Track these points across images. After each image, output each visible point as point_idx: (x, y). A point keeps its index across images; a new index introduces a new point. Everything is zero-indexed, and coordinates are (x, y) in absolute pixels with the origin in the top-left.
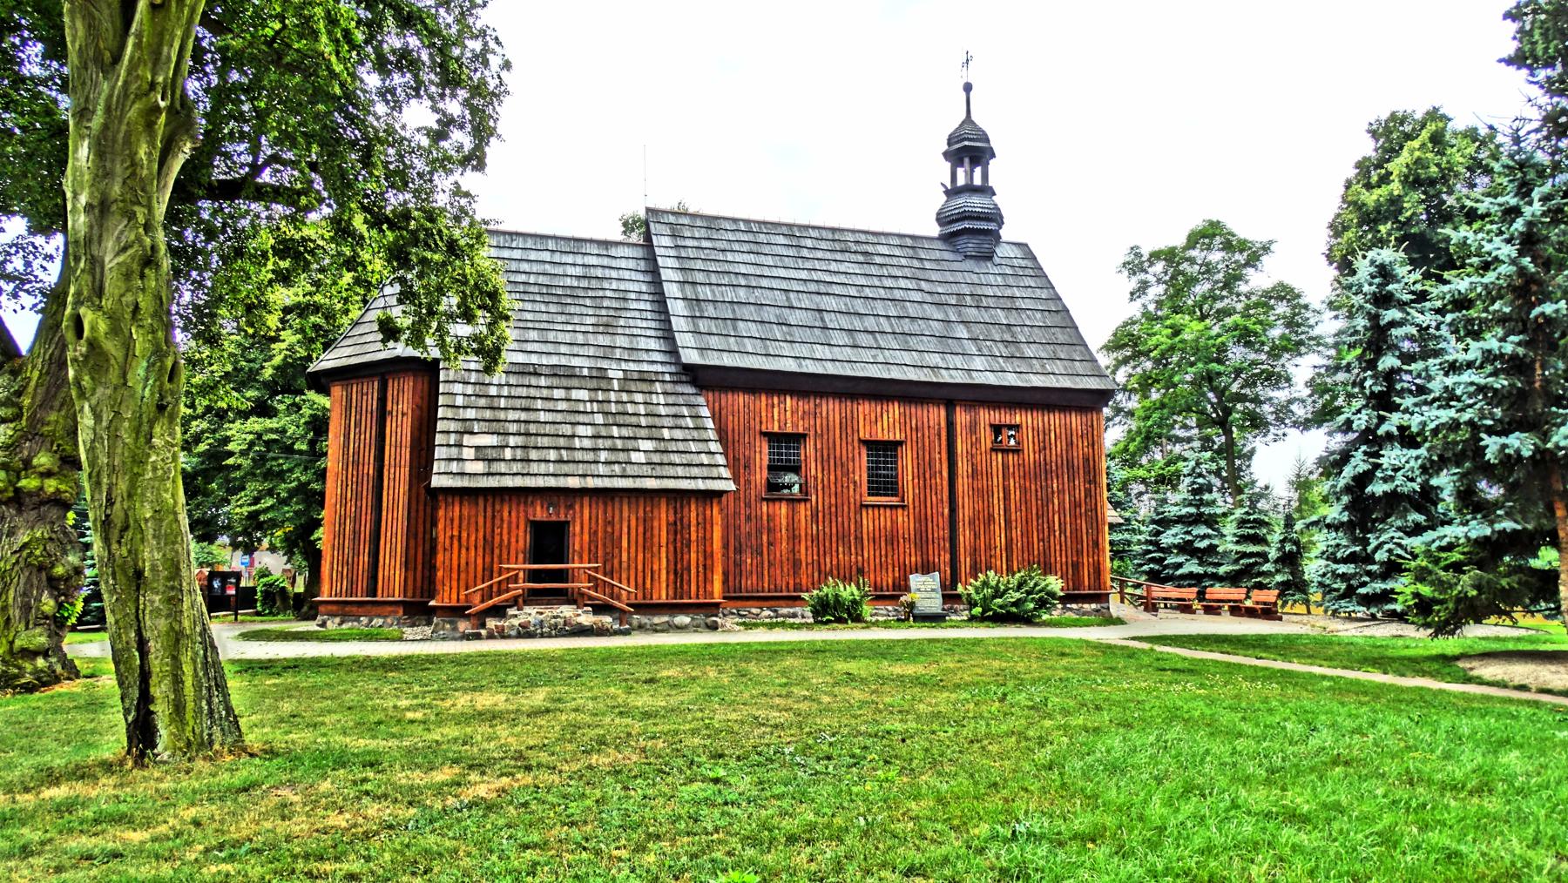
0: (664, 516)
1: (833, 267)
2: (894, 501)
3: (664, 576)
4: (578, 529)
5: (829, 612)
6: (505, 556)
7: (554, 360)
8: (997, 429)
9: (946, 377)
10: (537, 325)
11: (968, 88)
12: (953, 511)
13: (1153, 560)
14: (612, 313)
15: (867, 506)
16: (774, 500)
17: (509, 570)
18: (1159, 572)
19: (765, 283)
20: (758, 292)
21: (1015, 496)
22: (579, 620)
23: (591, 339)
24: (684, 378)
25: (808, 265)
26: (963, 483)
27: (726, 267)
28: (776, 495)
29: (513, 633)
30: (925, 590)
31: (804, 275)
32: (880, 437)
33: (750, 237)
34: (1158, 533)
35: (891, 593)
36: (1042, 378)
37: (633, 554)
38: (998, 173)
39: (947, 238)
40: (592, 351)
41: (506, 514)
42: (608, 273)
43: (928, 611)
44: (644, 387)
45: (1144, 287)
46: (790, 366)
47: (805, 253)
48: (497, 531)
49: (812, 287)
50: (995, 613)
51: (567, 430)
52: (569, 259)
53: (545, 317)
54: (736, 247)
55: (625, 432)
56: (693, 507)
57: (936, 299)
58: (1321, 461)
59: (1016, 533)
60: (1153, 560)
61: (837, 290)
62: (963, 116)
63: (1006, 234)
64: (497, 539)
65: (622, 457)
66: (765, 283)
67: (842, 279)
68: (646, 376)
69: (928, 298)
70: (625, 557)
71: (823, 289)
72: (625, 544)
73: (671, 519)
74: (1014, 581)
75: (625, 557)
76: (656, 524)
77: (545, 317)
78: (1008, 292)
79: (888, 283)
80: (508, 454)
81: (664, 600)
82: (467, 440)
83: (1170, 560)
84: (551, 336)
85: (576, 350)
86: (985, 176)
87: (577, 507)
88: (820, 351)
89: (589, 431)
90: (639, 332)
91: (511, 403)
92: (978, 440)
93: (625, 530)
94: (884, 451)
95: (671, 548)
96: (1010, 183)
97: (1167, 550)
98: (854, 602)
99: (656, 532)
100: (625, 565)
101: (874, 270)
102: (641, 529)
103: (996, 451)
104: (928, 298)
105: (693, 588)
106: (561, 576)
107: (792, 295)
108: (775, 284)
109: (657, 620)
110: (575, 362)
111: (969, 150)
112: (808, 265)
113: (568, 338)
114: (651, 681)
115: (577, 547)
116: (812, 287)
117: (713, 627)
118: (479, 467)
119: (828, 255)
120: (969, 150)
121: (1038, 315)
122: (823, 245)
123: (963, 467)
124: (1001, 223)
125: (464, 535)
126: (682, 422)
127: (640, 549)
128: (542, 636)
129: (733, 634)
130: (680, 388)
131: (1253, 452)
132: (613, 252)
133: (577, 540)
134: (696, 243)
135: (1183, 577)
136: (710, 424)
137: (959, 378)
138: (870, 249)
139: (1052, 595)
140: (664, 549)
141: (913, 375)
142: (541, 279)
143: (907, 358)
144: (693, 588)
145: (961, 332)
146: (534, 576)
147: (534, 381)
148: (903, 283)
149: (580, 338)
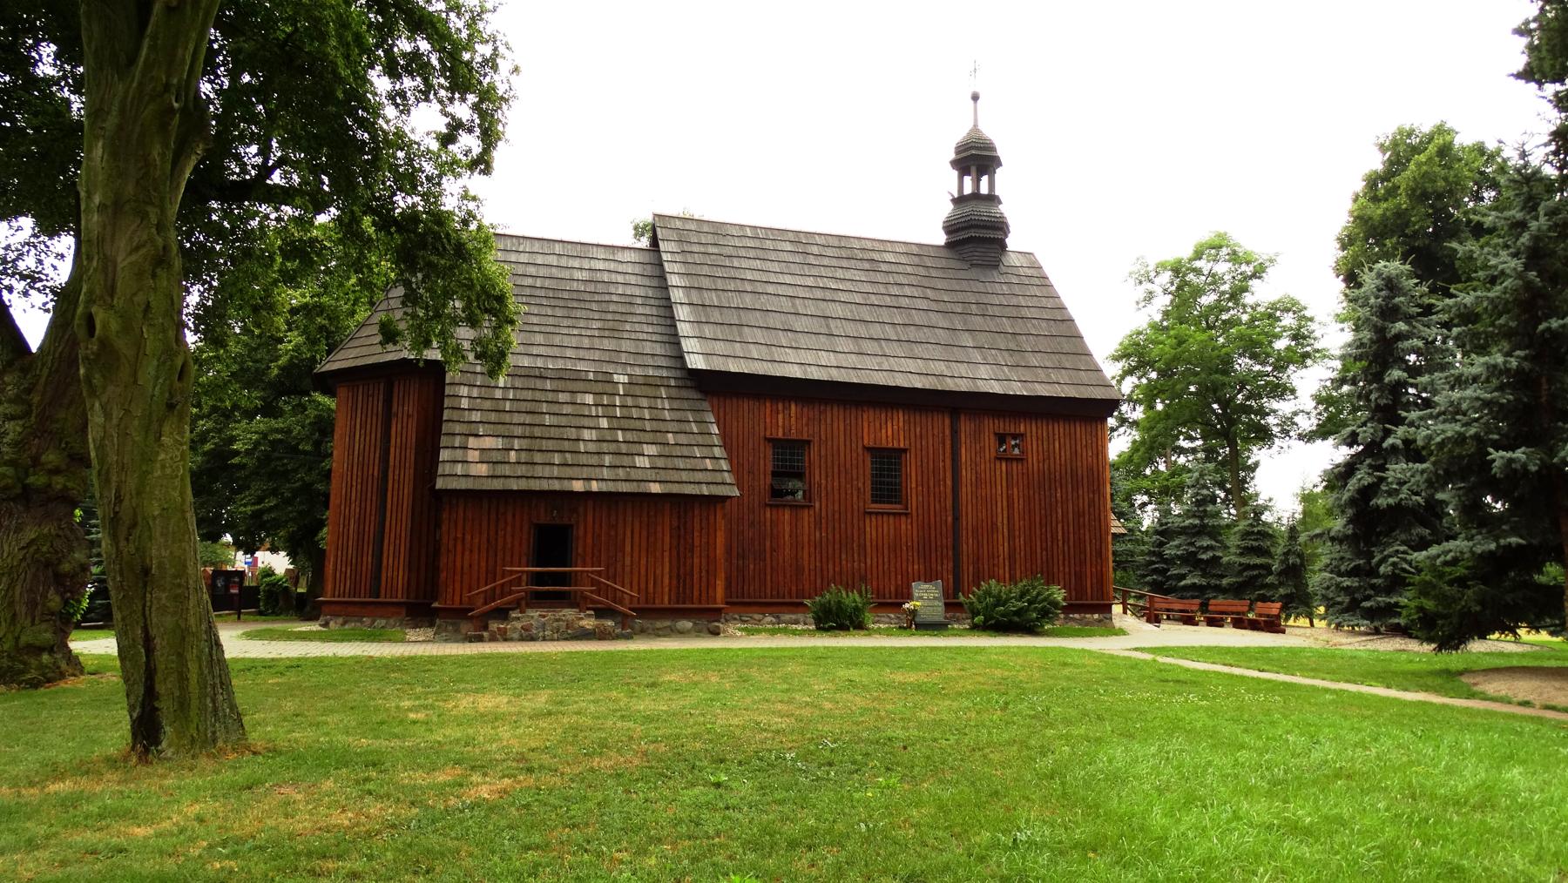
0: (667, 519)
1: (840, 274)
2: (897, 508)
3: (666, 581)
4: (581, 533)
5: (836, 620)
6: (508, 558)
7: (560, 364)
10: (543, 329)
11: (975, 98)
12: (956, 519)
13: (1155, 571)
14: (618, 317)
16: (777, 506)
17: (512, 572)
18: (1163, 583)
19: (770, 289)
20: (763, 298)
21: (1019, 505)
22: (583, 623)
23: (597, 343)
24: (689, 383)
25: (814, 271)
26: (965, 491)
27: (733, 273)
28: (778, 501)
29: (516, 636)
30: (926, 597)
31: (810, 282)
32: (884, 445)
33: (757, 243)
34: (1161, 544)
36: (1048, 387)
39: (949, 245)
40: (597, 355)
41: (510, 518)
42: (614, 277)
43: (930, 619)
44: (650, 391)
45: (1150, 297)
46: (795, 372)
47: (812, 260)
48: (501, 533)
49: (819, 294)
50: (998, 621)
51: (572, 433)
52: (576, 263)
53: (551, 321)
54: (743, 253)
55: (630, 436)
57: (942, 307)
59: (1020, 542)
60: (1155, 571)
61: (843, 297)
62: (971, 126)
63: (1012, 243)
64: (500, 541)
65: (626, 461)
66: (770, 289)
67: (848, 286)
68: (651, 381)
69: (934, 306)
70: (628, 562)
71: (828, 295)
72: (628, 549)
73: (675, 524)
74: (1016, 591)
75: (628, 562)
76: (659, 529)
77: (551, 321)
78: (1014, 301)
79: (895, 290)
80: (513, 456)
81: (666, 605)
82: (472, 442)
83: (1173, 571)
84: (557, 340)
85: (582, 354)
87: (581, 510)
89: (593, 435)
90: (645, 336)
91: (516, 406)
92: (983, 449)
94: (887, 461)
96: (1012, 191)
97: (1170, 561)
98: (856, 609)
99: (659, 535)
100: (628, 569)
101: (879, 278)
102: (644, 533)
103: (1000, 459)
104: (934, 306)
105: (696, 593)
106: (563, 579)
107: (797, 301)
108: (781, 290)
109: (659, 624)
110: (581, 366)
111: (976, 159)
112: (814, 271)
113: (574, 342)
116: (819, 294)
117: (715, 633)
118: (483, 469)
119: (834, 262)
120: (976, 159)
121: (1044, 324)
122: (829, 252)
125: (468, 537)
126: (685, 427)
127: (643, 554)
128: (544, 639)
129: (737, 641)
131: (1257, 464)
132: (619, 256)
134: (702, 249)
135: (1186, 588)
137: (964, 386)
138: (876, 256)
139: (1055, 604)
140: (667, 554)
141: (918, 383)
142: (547, 283)
143: (911, 365)
144: (696, 593)
145: (967, 340)
146: (538, 579)
147: (539, 384)
148: (908, 291)
149: (586, 342)
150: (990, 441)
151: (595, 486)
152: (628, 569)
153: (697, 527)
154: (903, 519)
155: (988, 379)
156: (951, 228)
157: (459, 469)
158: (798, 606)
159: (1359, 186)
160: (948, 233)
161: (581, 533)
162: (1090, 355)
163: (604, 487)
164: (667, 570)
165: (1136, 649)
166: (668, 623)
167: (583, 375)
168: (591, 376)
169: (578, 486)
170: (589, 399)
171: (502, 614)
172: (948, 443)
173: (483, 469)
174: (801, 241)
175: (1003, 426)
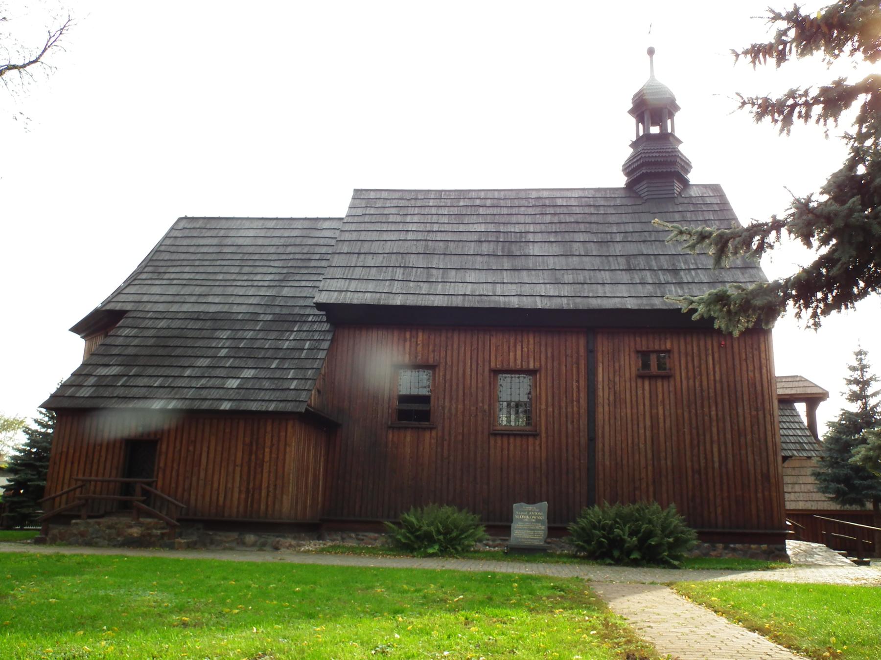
3: (236, 495)
7: (218, 308)
8: (644, 355)
9: (595, 303)
11: (651, 52)
15: (495, 435)
16: (399, 428)
20: (366, 245)
26: (603, 412)
30: (528, 522)
35: (500, 526)
37: (210, 472)
38: (682, 126)
56: (269, 429)
58: (825, 91)
63: (694, 178)
73: (248, 440)
84: (230, 290)
86: (663, 128)
88: (425, 288)
90: (308, 284)
93: (205, 449)
95: (246, 469)
100: (201, 483)
102: (219, 448)
108: (439, 237)
110: (235, 309)
111: (652, 109)
114: (652, 583)
115: (162, 465)
120: (652, 109)
123: (603, 394)
124: (686, 166)
131: (809, 245)
133: (163, 457)
140: (238, 469)
150: (629, 364)
152: (201, 483)
153: (268, 443)
154: (531, 439)
156: (630, 169)
158: (376, 526)
160: (628, 174)
161: (164, 447)
164: (237, 484)
166: (235, 535)
170: (225, 334)
171: (64, 518)
172: (582, 363)
174: (440, 194)
175: (643, 343)
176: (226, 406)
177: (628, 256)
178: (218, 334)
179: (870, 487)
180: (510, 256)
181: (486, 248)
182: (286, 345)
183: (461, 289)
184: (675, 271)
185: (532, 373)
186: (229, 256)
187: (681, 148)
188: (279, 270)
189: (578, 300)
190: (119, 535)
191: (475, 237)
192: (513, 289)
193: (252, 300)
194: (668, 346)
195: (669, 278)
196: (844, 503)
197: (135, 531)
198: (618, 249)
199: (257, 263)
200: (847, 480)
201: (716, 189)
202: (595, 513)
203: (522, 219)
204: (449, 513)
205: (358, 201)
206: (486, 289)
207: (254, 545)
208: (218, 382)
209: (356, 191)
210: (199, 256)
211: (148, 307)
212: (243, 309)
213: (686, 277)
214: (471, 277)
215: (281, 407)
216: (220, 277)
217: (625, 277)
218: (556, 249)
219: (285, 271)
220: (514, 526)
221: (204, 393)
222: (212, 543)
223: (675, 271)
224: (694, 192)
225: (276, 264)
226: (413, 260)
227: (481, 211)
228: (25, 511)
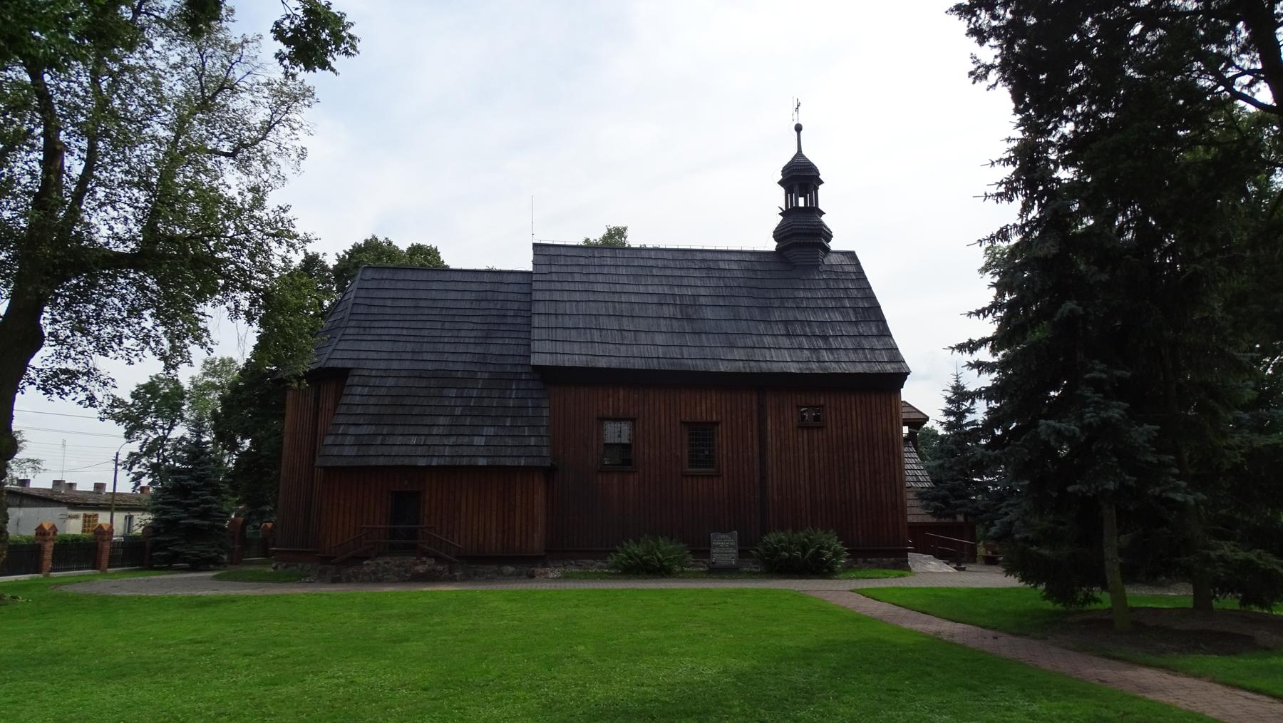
9: (765, 367)
11: (798, 128)
20: (561, 305)
30: (724, 546)
35: (701, 550)
63: (834, 245)
94: (701, 432)
110: (451, 366)
111: (801, 178)
117: (531, 576)
120: (801, 178)
124: (829, 236)
130: (531, 385)
136: (546, 413)
151: (435, 462)
155: (786, 359)
156: (778, 235)
157: (335, 451)
159: (348, 248)
162: (891, 336)
163: (442, 462)
165: (233, 601)
166: (495, 567)
167: (454, 374)
168: (459, 375)
169: (422, 462)
170: (453, 393)
171: (358, 559)
173: (352, 451)
176: (482, 462)
177: (786, 323)
178: (446, 392)
179: (961, 506)
180: (689, 319)
181: (667, 311)
182: (511, 403)
183: (653, 352)
184: (825, 338)
185: (633, 420)
186: (426, 311)
187: (823, 218)
188: (479, 327)
189: (753, 364)
190: (406, 571)
191: (655, 300)
192: (695, 352)
193: (464, 358)
194: (822, 402)
195: (821, 343)
196: (940, 517)
197: (420, 569)
198: (777, 315)
199: (457, 319)
200: (944, 500)
201: (851, 255)
202: (772, 538)
203: (692, 282)
204: (665, 545)
205: (541, 258)
206: (675, 352)
207: (512, 575)
208: (466, 440)
209: (535, 245)
210: (397, 311)
211: (369, 364)
212: (459, 367)
213: (834, 344)
214: (660, 339)
215: (531, 462)
216: (426, 333)
217: (785, 342)
218: (723, 313)
219: (485, 327)
220: (713, 551)
221: (460, 451)
222: (475, 574)
223: (825, 338)
224: (833, 259)
225: (475, 320)
226: (605, 322)
227: (655, 272)
228: (177, 549)
